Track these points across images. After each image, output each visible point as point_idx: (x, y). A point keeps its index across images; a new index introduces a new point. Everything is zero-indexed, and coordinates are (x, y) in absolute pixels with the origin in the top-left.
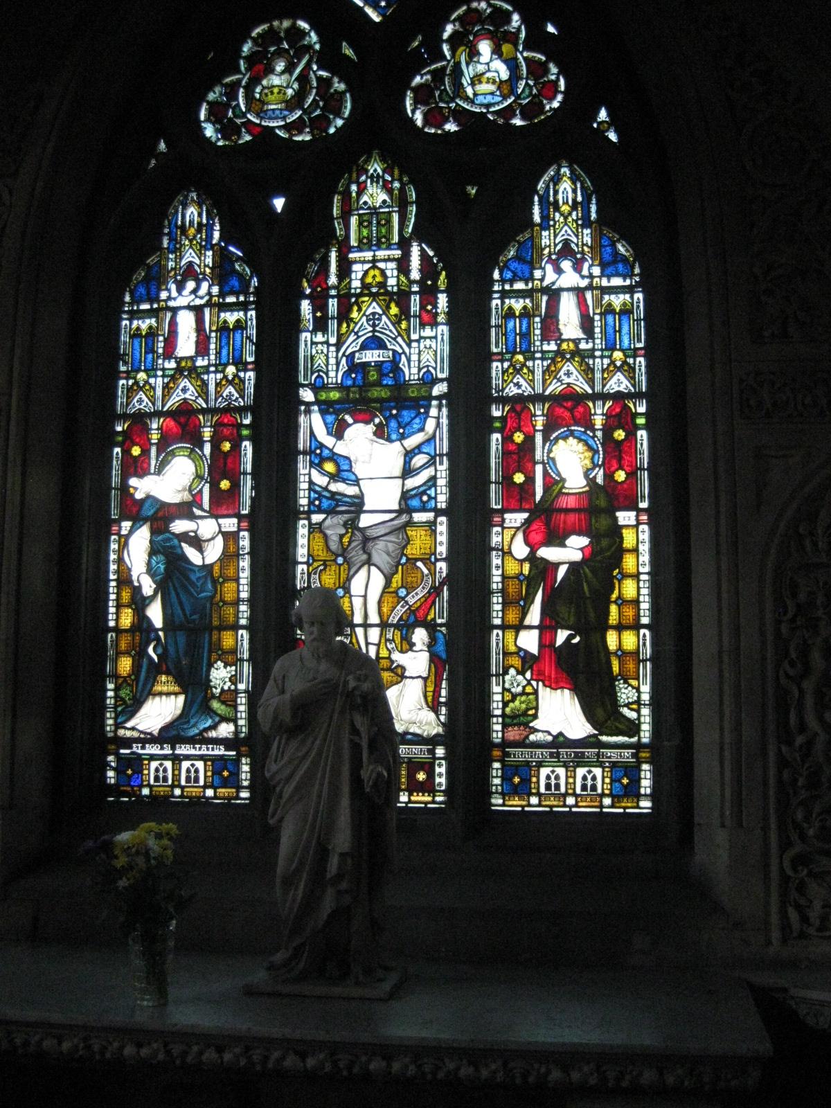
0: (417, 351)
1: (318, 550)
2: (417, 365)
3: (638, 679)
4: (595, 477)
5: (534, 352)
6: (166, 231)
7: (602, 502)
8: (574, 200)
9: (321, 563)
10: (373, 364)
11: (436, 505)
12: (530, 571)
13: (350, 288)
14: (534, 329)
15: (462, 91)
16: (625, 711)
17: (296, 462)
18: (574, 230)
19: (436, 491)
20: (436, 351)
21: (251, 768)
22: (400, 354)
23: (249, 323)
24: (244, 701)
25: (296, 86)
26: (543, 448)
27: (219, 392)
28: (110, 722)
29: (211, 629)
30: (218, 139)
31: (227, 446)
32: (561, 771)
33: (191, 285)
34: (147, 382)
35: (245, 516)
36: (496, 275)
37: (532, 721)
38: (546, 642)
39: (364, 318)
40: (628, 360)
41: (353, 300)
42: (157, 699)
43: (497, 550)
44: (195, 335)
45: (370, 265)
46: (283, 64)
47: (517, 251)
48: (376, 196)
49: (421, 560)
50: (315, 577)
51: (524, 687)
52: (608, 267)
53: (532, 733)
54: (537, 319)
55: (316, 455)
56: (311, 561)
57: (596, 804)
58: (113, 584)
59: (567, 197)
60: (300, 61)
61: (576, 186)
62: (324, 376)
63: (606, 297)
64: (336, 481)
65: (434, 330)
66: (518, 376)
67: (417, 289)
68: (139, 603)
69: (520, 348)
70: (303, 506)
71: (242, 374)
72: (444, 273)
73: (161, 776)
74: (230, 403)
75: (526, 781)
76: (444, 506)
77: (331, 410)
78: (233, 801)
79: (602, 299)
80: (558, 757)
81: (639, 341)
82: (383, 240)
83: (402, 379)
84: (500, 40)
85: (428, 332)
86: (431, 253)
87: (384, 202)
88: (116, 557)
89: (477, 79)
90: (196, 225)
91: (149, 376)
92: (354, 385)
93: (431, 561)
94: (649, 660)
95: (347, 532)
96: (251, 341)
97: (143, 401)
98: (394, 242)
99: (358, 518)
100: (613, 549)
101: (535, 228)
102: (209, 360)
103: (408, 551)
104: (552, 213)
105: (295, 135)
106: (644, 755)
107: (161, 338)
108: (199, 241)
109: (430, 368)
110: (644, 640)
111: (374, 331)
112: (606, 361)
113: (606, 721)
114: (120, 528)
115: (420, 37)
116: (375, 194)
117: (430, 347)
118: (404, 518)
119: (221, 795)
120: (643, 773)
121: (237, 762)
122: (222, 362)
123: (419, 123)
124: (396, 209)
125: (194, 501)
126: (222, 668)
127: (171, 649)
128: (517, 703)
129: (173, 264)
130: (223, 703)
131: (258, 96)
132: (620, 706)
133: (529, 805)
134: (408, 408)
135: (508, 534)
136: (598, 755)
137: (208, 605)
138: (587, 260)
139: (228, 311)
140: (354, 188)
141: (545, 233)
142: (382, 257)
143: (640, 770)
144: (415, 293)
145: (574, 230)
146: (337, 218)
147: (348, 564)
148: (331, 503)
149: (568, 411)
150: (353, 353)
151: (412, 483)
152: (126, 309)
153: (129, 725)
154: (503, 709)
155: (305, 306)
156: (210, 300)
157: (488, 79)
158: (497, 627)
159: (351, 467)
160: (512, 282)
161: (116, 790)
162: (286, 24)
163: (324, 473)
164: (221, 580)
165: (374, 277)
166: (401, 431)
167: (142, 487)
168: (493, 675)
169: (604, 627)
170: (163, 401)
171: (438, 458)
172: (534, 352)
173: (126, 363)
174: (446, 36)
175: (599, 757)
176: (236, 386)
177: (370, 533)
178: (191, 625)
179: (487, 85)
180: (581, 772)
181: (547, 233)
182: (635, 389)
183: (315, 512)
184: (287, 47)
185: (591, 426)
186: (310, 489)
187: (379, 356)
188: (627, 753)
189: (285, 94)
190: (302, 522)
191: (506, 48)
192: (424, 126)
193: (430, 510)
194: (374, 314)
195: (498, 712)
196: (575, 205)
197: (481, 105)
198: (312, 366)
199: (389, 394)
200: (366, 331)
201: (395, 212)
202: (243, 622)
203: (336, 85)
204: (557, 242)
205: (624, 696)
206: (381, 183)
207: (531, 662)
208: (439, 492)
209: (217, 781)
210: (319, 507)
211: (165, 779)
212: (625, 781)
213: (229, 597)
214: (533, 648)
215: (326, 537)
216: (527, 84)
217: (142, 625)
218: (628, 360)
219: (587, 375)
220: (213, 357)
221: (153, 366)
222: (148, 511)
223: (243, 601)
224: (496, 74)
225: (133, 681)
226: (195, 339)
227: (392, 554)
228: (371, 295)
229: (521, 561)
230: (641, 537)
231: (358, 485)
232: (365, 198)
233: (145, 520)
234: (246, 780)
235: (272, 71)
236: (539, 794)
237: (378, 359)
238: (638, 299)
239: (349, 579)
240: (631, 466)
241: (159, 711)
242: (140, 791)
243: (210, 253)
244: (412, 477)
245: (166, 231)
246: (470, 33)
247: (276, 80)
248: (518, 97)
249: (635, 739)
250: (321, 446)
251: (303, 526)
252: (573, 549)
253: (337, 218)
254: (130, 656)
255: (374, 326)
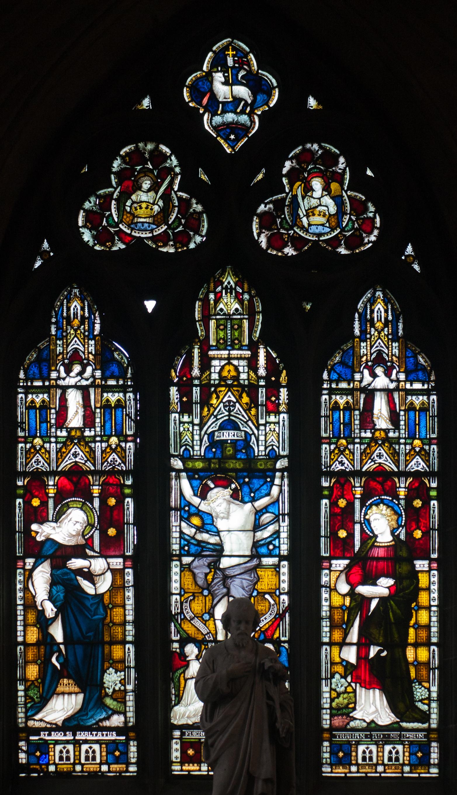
0: (264, 433)
1: (188, 585)
2: (264, 444)
3: (429, 682)
4: (399, 534)
5: (355, 438)
6: (54, 320)
7: (404, 553)
8: (386, 318)
9: (191, 594)
10: (229, 441)
11: (280, 553)
12: (350, 603)
13: (210, 380)
14: (354, 420)
15: (298, 220)
16: (420, 705)
17: (169, 516)
18: (386, 343)
19: (279, 541)
20: (279, 434)
21: (137, 749)
22: (251, 435)
23: (128, 403)
24: (131, 698)
25: (161, 203)
26: (361, 512)
27: (104, 458)
28: (21, 715)
29: (103, 643)
30: (95, 245)
31: (112, 502)
32: (374, 748)
33: (77, 368)
34: (42, 447)
35: (129, 557)
36: (325, 376)
37: (352, 712)
38: (362, 655)
39: (222, 405)
40: (425, 447)
41: (213, 389)
42: (61, 697)
43: (326, 587)
44: (83, 410)
45: (226, 361)
46: (149, 182)
47: (342, 357)
48: (229, 304)
49: (269, 593)
50: (186, 605)
51: (346, 688)
52: (412, 374)
53: (352, 721)
54: (357, 412)
55: (185, 511)
56: (183, 593)
57: (399, 771)
58: (20, 608)
59: (381, 316)
60: (163, 181)
61: (387, 307)
62: (191, 449)
63: (409, 398)
64: (201, 532)
65: (277, 417)
66: (342, 456)
67: (263, 384)
68: (43, 623)
69: (344, 434)
70: (176, 550)
71: (123, 445)
72: (284, 371)
73: (65, 757)
74: (114, 467)
75: (348, 755)
76: (286, 553)
77: (197, 476)
78: (123, 774)
79: (406, 399)
80: (371, 738)
81: (433, 432)
82: (236, 342)
83: (252, 455)
84: (330, 178)
85: (272, 418)
86: (274, 355)
87: (237, 310)
88: (22, 586)
89: (310, 212)
90: (79, 318)
91: (44, 442)
92: (214, 458)
93: (276, 595)
94: (437, 668)
95: (211, 572)
96: (130, 418)
97: (40, 462)
98: (244, 344)
99: (219, 561)
100: (412, 587)
101: (356, 340)
102: (95, 431)
103: (259, 586)
104: (368, 328)
105: (161, 247)
106: (433, 736)
107: (53, 411)
108: (83, 331)
109: (274, 447)
110: (434, 654)
111: (229, 415)
112: (408, 447)
113: (406, 712)
114: (25, 564)
115: (264, 170)
116: (229, 303)
117: (274, 430)
118: (255, 562)
119: (114, 770)
120: (432, 749)
121: (126, 744)
122: (106, 434)
123: (264, 245)
124: (246, 317)
125: (86, 544)
126: (113, 673)
127: (71, 658)
128: (341, 699)
129: (61, 349)
130: (115, 700)
131: (128, 209)
132: (416, 701)
133: (350, 772)
134: (259, 478)
135: (334, 575)
136: (400, 736)
137: (101, 625)
138: (395, 368)
139: (110, 392)
140: (212, 296)
141: (363, 344)
142: (236, 356)
143: (430, 747)
144: (262, 386)
145: (386, 343)
146: (198, 321)
147: (212, 596)
148: (199, 549)
149: (379, 484)
150: (214, 432)
151: (260, 535)
152: (21, 384)
153: (37, 717)
154: (331, 703)
155: (174, 391)
156: (94, 381)
157: (320, 212)
158: (326, 644)
159: (213, 521)
160: (337, 382)
161: (26, 768)
162: (150, 147)
163: (191, 526)
164: (110, 606)
165: (229, 372)
166: (252, 495)
167: (43, 531)
168: (323, 679)
169: (405, 644)
170: (57, 462)
171: (281, 517)
172: (355, 438)
173: (23, 430)
174: (285, 171)
175: (400, 738)
176: (120, 453)
177: (227, 573)
178: (87, 640)
179: (319, 217)
180: (388, 748)
181: (365, 344)
182: (429, 469)
183: (185, 555)
184: (151, 167)
185: (396, 496)
186: (181, 538)
187: (234, 435)
188: (421, 735)
189: (152, 209)
190: (174, 563)
191: (334, 186)
192: (268, 248)
193: (275, 556)
194: (229, 401)
195: (327, 706)
196: (386, 323)
197: (314, 234)
198: (181, 441)
199: (242, 465)
200: (223, 415)
201: (246, 319)
202: (129, 638)
203: (195, 206)
204: (372, 352)
205: (419, 694)
206: (234, 294)
207: (351, 670)
208: (282, 542)
209: (110, 759)
210: (188, 551)
211: (68, 758)
212: (420, 754)
213: (118, 619)
214: (353, 659)
215: (194, 575)
216: (350, 219)
217: (46, 641)
218: (425, 447)
219: (394, 457)
220: (98, 429)
221: (47, 433)
222: (48, 550)
223: (129, 622)
224: (326, 208)
225: (39, 683)
226: (82, 414)
227: (247, 589)
228: (226, 385)
229: (344, 596)
230: (432, 579)
231: (219, 535)
232: (221, 306)
233: (46, 558)
234: (134, 758)
235: (140, 188)
236: (357, 764)
237: (233, 438)
238: (433, 400)
239: (213, 607)
240: (426, 527)
241: (62, 707)
242: (48, 768)
243: (92, 342)
244: (261, 530)
245: (54, 320)
246: (305, 170)
247: (144, 197)
248: (343, 230)
249: (426, 725)
250: (189, 504)
251: (176, 566)
252: (383, 587)
253: (198, 321)
254: (37, 664)
255: (229, 411)
